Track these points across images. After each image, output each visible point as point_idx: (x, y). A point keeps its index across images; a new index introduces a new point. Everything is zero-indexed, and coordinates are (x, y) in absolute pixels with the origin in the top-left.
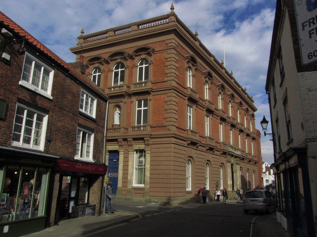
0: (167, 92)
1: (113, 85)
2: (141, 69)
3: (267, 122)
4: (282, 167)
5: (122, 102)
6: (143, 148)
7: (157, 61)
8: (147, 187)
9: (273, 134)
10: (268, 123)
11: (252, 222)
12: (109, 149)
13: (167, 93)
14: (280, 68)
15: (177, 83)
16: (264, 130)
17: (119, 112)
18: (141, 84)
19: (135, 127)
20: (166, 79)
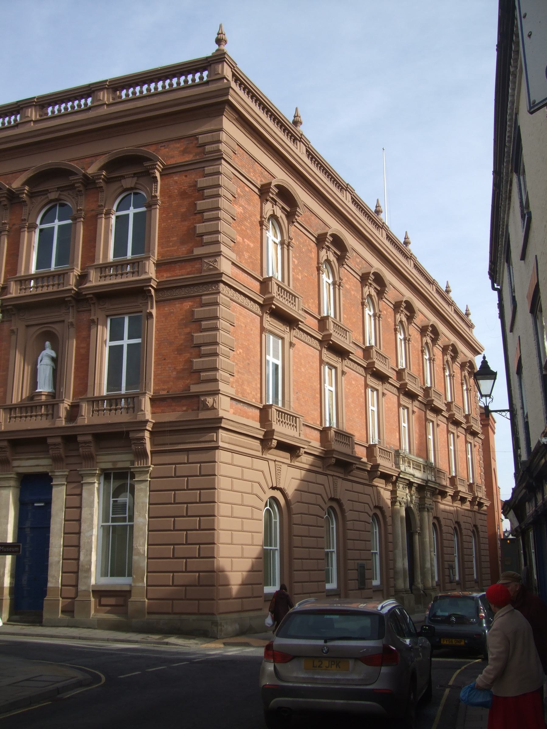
2: (122, 221)
3: (492, 375)
4: (530, 509)
6: (128, 465)
7: (170, 197)
8: (140, 584)
9: (512, 410)
10: (495, 379)
11: (451, 683)
12: (21, 470)
14: (521, 202)
15: (233, 264)
16: (484, 398)
17: (53, 354)
18: (122, 265)
19: (102, 399)
20: (198, 251)
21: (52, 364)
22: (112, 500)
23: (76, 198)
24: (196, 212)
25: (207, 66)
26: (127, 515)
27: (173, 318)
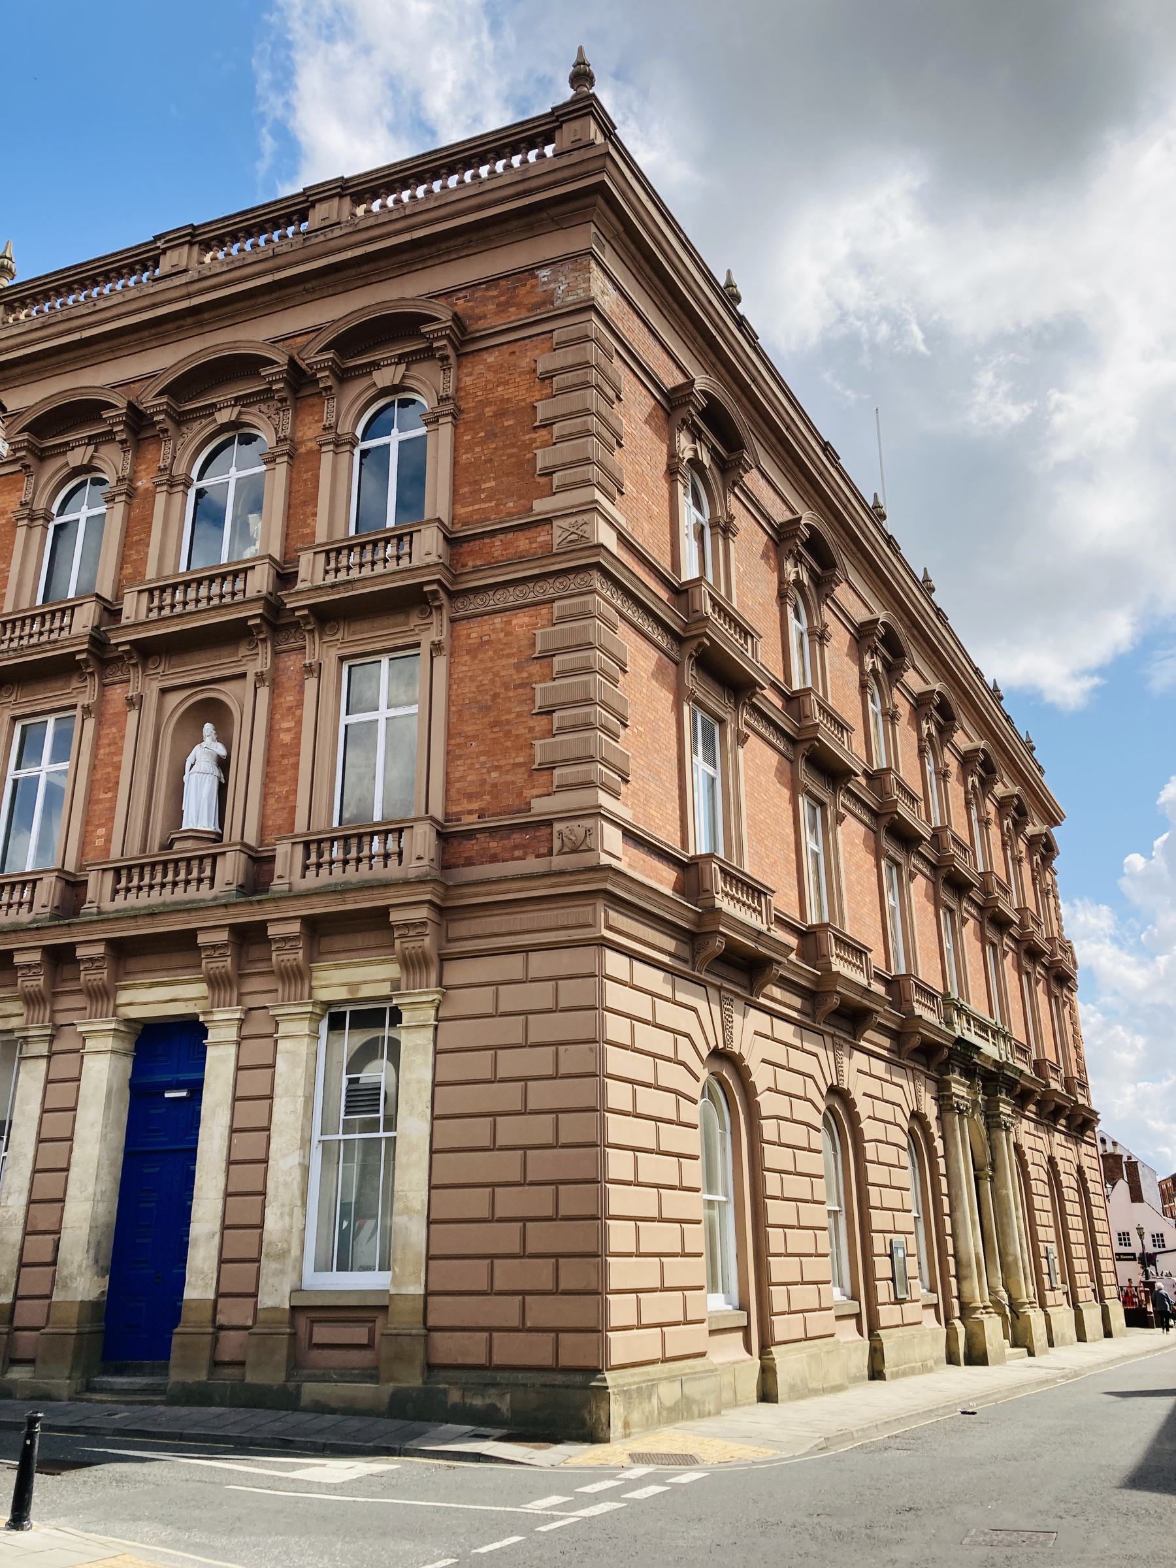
0: (550, 589)
1: (391, 522)
5: (243, 676)
6: (385, 989)
13: (553, 601)
17: (221, 750)
20: (542, 506)
21: (217, 772)
22: (345, 1079)
23: (275, 417)
24: (537, 424)
25: (554, 130)
26: (381, 1114)
27: (490, 653)
